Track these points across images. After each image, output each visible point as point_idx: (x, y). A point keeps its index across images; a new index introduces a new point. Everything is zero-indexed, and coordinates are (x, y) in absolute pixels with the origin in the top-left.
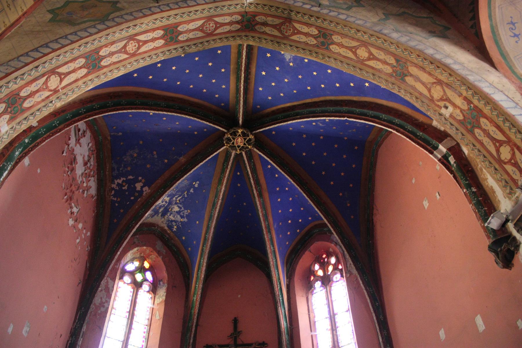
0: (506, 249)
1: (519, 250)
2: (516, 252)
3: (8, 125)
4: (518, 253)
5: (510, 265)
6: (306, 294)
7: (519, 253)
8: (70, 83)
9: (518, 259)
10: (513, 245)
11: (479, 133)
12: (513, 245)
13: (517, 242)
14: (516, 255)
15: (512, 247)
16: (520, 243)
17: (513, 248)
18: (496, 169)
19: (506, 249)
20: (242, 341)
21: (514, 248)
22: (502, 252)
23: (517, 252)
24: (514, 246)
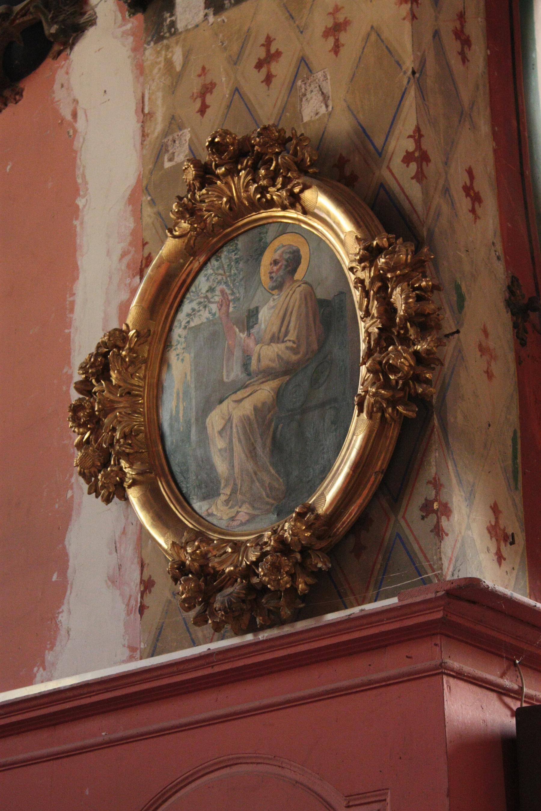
0: (26, 18)
1: (72, 47)
2: (56, 48)
3: (341, 154)
4: (63, 55)
5: (7, 93)
6: (135, 50)
7: (67, 58)
8: (333, 689)
9: (51, 81)
10: (61, 18)
11: (331, 41)
12: (61, 18)
13: (83, 14)
14: (49, 61)
15: (53, 21)
16: (92, 22)
17: (53, 30)
18: (459, 571)
19: (26, 18)
20: (234, 94)
21: (61, 31)
22: (7, 24)
23: (59, 53)
24: (64, 20)
